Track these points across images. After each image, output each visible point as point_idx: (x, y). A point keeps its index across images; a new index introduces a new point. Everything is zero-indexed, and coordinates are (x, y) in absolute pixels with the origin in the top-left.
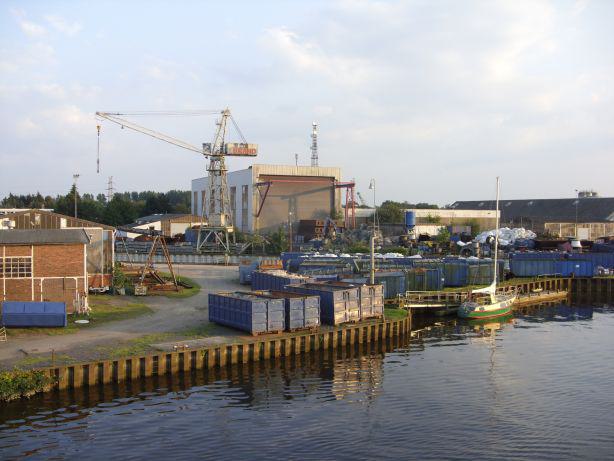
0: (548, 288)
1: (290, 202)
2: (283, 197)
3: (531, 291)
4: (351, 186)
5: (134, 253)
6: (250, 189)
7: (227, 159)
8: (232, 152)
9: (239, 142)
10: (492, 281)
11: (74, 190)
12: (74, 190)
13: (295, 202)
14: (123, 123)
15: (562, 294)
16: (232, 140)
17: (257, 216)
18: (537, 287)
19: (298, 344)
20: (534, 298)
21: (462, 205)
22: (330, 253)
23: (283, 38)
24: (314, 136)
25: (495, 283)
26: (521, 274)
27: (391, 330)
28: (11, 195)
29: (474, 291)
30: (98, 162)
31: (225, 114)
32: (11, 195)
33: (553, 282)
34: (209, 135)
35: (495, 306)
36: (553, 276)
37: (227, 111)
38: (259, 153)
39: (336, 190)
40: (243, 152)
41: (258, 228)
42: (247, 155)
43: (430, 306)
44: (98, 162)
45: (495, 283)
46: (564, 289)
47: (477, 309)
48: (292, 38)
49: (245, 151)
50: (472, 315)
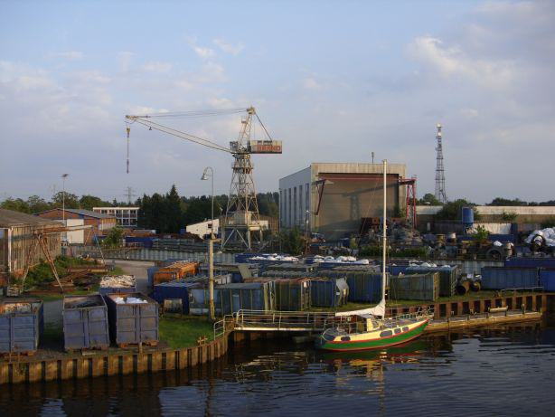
0: (344, 319)
1: (352, 199)
2: (344, 195)
3: (486, 311)
4: (412, 182)
5: (164, 250)
6: (311, 187)
7: (253, 156)
8: (256, 149)
9: (263, 139)
10: (380, 299)
11: (173, 190)
12: (173, 190)
13: (357, 199)
14: (152, 125)
15: (534, 315)
16: (257, 134)
17: (317, 214)
18: (498, 304)
19: (204, 355)
20: (493, 319)
21: (498, 202)
22: (325, 254)
23: (428, 45)
24: (439, 138)
25: (384, 300)
26: (491, 287)
27: (213, 352)
28: (145, 196)
29: (338, 314)
30: (128, 163)
31: (251, 111)
32: (145, 196)
33: (529, 299)
34: (234, 129)
35: (372, 334)
36: (530, 291)
37: (252, 108)
38: (283, 150)
39: (401, 187)
40: (266, 149)
41: (318, 225)
42: (271, 152)
43: (291, 329)
44: (128, 163)
45: (384, 300)
46: (538, 310)
47: (338, 339)
48: (436, 43)
49: (269, 148)
50: (328, 346)
